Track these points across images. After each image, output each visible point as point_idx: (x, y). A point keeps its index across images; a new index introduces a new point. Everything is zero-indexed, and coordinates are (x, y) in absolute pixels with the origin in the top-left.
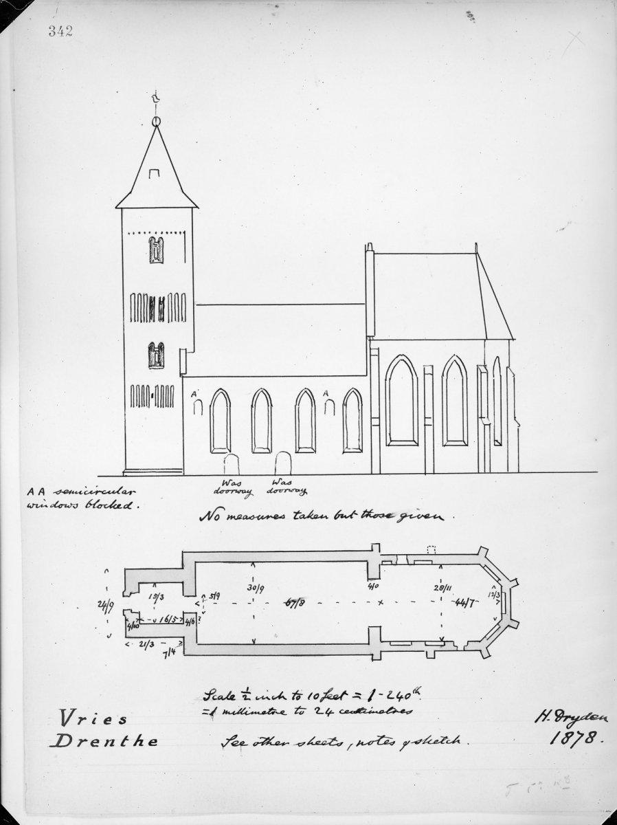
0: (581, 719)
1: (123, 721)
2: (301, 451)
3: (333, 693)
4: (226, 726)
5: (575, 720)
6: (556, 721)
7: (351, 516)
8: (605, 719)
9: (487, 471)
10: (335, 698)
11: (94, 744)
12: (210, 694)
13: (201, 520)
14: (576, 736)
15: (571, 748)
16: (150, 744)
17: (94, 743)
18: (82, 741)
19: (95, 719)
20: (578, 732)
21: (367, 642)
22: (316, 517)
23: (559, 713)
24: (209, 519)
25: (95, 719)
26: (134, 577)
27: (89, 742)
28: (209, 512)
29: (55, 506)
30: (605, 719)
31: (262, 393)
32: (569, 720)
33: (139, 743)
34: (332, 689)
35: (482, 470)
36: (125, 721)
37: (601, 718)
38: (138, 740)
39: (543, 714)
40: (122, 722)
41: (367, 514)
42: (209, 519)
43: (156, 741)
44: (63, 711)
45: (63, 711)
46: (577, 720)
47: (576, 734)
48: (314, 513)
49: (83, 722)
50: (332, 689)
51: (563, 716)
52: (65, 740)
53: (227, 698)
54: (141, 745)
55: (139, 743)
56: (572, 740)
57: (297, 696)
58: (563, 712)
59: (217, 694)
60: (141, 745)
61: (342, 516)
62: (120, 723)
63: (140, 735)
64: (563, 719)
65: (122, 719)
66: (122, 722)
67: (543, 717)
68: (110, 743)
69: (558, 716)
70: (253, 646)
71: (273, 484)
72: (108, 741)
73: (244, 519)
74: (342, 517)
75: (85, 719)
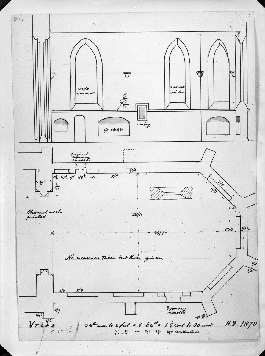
2: (171, 107)
3: (125, 324)
7: (125, 258)
10: (126, 326)
13: (66, 259)
14: (250, 323)
19: (42, 325)
20: (250, 322)
21: (215, 152)
22: (111, 258)
24: (69, 259)
25: (42, 325)
26: (148, 105)
28: (70, 256)
31: (177, 50)
34: (124, 323)
36: (54, 326)
39: (228, 323)
40: (53, 326)
41: (131, 257)
42: (69, 259)
44: (30, 322)
45: (30, 322)
47: (249, 322)
48: (111, 257)
49: (37, 326)
50: (124, 323)
56: (248, 325)
61: (122, 258)
62: (52, 327)
65: (53, 325)
66: (53, 326)
67: (228, 324)
73: (84, 259)
74: (122, 259)
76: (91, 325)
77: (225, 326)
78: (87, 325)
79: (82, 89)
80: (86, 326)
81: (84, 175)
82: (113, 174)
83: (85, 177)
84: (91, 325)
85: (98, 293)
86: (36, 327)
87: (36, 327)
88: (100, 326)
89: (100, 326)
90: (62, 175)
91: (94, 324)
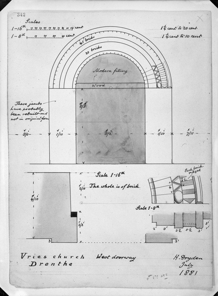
0: (192, 259)
1: (45, 257)
4: (188, 274)
8: (202, 259)
9: (62, 86)
11: (46, 265)
12: (28, 21)
15: (167, 278)
16: (70, 265)
29: (114, 258)
32: (187, 259)
38: (65, 264)
43: (48, 264)
51: (185, 258)
53: (34, 22)
54: (66, 265)
58: (184, 256)
59: (30, 21)
60: (66, 265)
62: (44, 258)
64: (185, 258)
65: (45, 257)
68: (53, 264)
69: (182, 258)
72: (52, 264)
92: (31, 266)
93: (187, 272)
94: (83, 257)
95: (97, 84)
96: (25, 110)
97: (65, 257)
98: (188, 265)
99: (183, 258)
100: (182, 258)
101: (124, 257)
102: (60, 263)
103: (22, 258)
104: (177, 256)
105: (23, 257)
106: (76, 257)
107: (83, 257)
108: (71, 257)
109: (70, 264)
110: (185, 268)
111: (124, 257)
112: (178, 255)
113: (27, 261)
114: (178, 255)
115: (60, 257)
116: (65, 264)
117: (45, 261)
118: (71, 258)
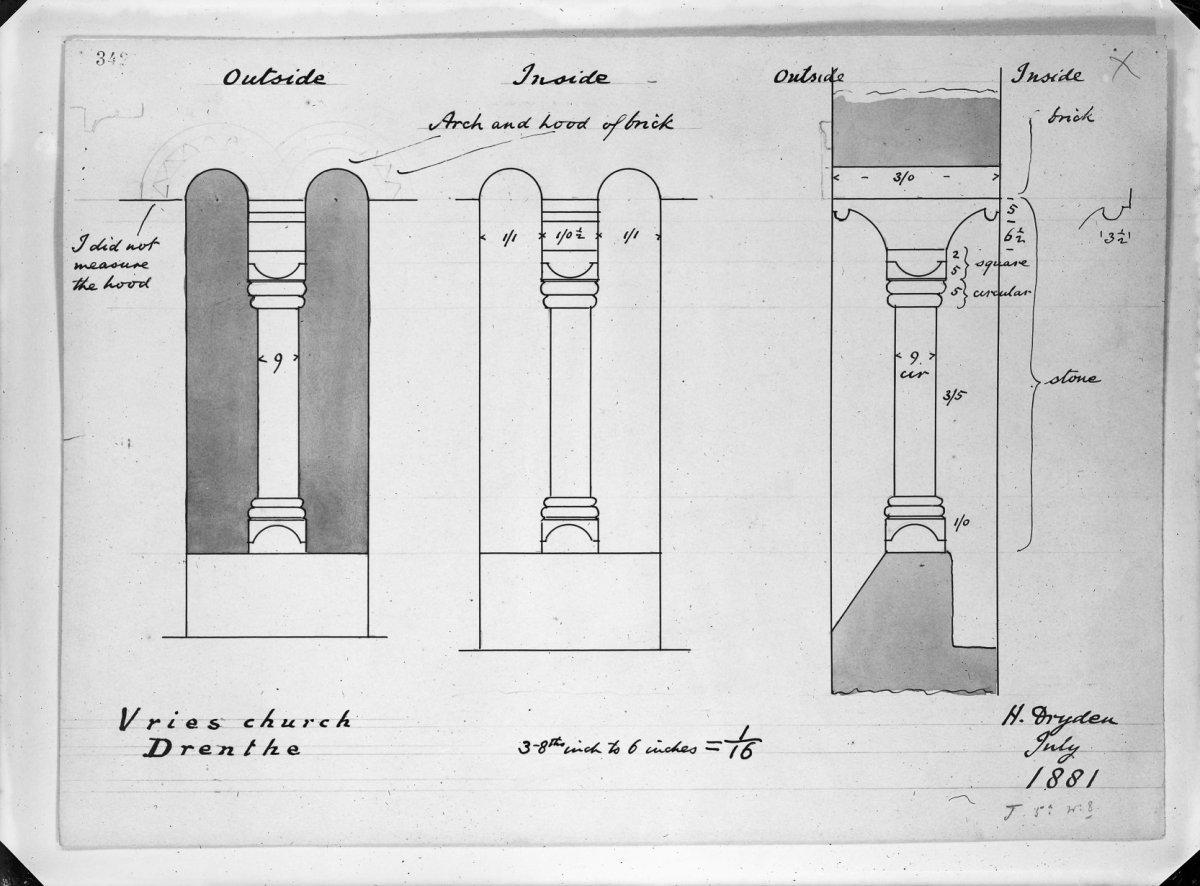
4: (1062, 781)
5: (1064, 721)
6: (1036, 723)
9: (546, 217)
17: (204, 751)
18: (185, 748)
19: (173, 721)
23: (1038, 712)
25: (173, 721)
27: (197, 750)
30: (1111, 721)
33: (268, 723)
35: (547, 206)
37: (1103, 721)
38: (267, 719)
39: (1011, 713)
46: (1067, 722)
49: (189, 750)
52: (162, 746)
55: (268, 723)
57: (742, 746)
58: (1044, 709)
62: (210, 727)
63: (273, 741)
65: (212, 722)
67: (1011, 718)
70: (883, 538)
71: (76, 268)
75: (158, 721)
76: (543, 747)
77: (1004, 723)
78: (527, 744)
79: (645, 127)
80: (525, 749)
81: (580, 231)
82: (69, 285)
83: (579, 237)
84: (543, 747)
85: (660, 553)
86: (183, 753)
87: (183, 753)
88: (574, 751)
89: (574, 751)
90: (562, 227)
91: (556, 742)
92: (151, 754)
93: (1058, 773)
94: (344, 721)
95: (156, 203)
96: (112, 287)
97: (286, 721)
98: (1061, 748)
99: (1040, 719)
100: (1038, 717)
101: (1055, 716)
102: (253, 744)
103: (123, 728)
104: (1015, 712)
105: (129, 723)
106: (246, 725)
107: (344, 721)
108: (307, 721)
109: (293, 751)
110: (1049, 761)
111: (1055, 716)
112: (1021, 708)
113: (139, 737)
114: (1021, 708)
115: (268, 721)
116: (272, 749)
117: (216, 739)
118: (305, 726)
